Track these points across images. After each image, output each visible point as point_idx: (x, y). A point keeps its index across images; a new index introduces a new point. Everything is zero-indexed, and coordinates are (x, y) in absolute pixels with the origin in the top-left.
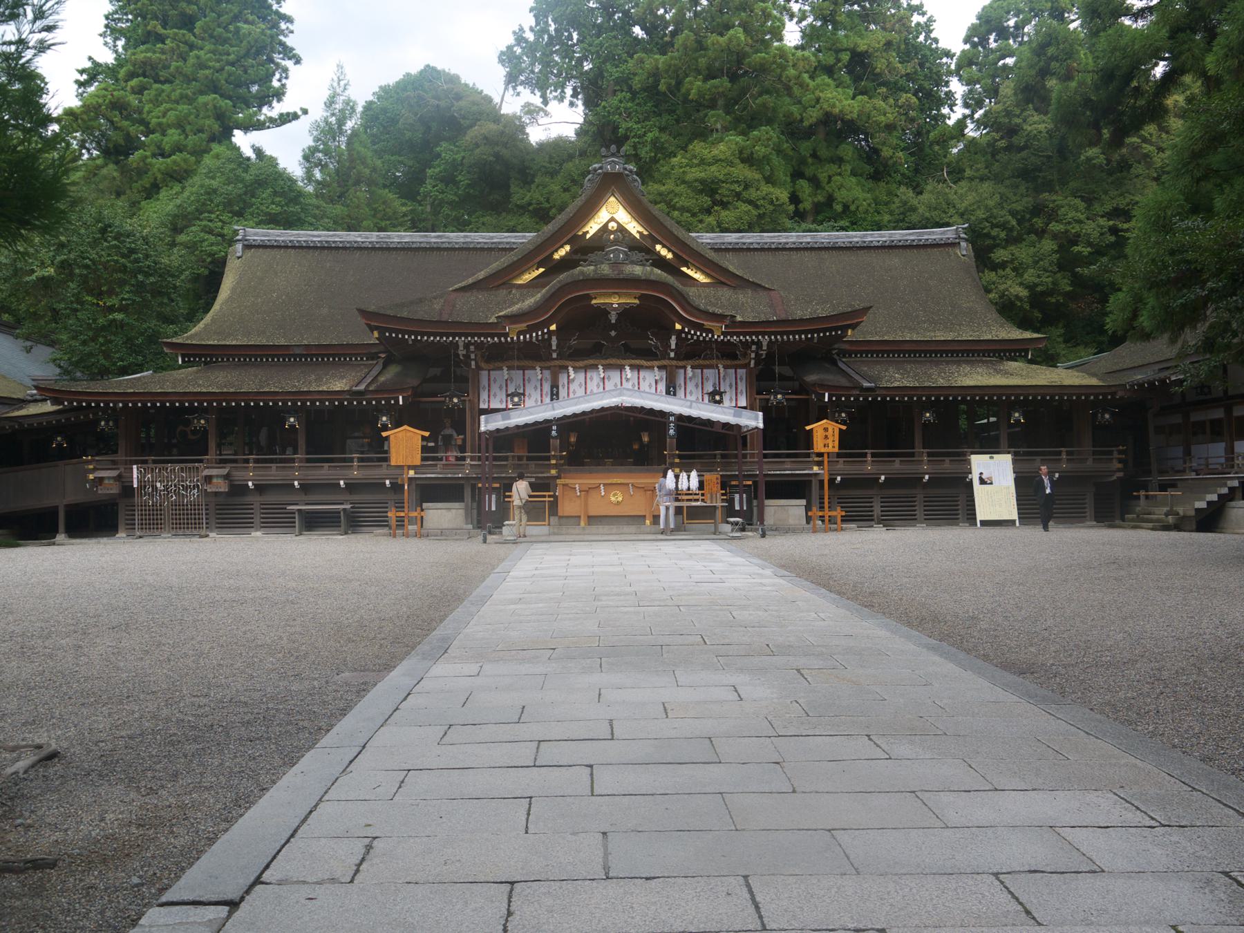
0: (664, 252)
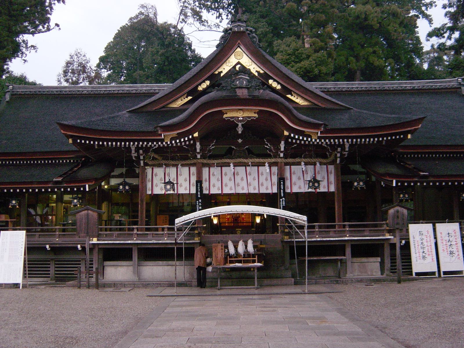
0: (275, 85)
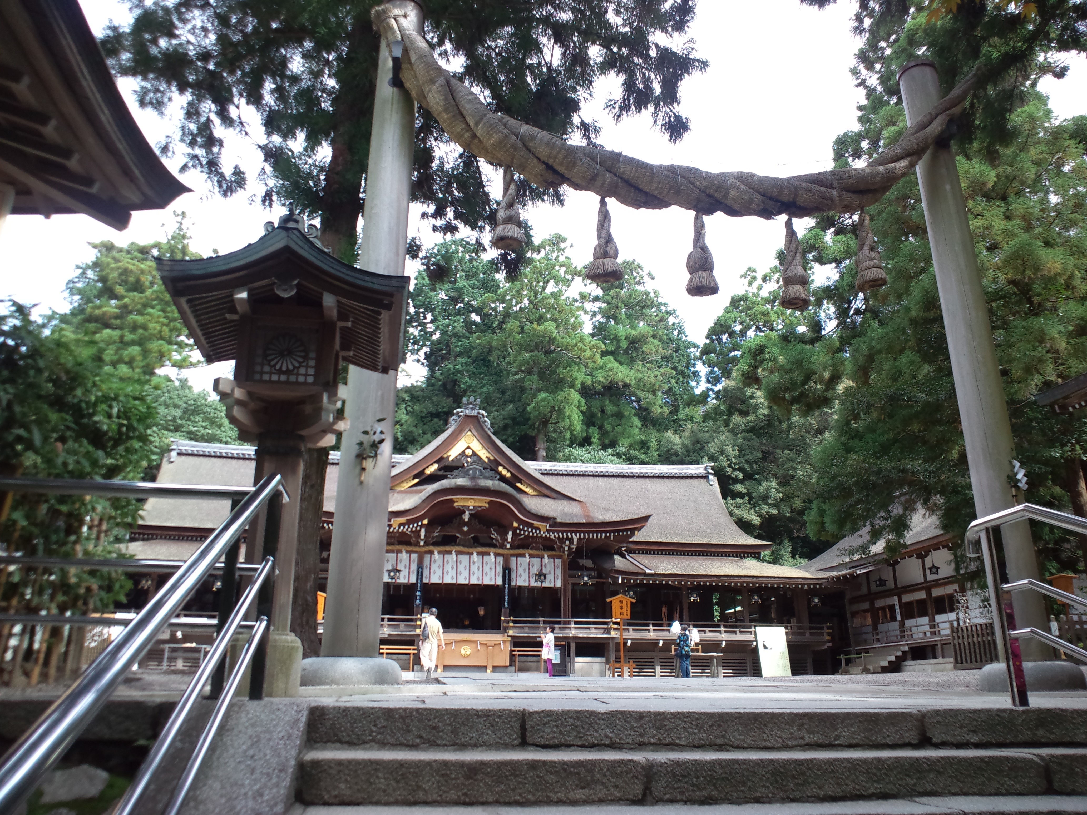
0: (504, 472)
